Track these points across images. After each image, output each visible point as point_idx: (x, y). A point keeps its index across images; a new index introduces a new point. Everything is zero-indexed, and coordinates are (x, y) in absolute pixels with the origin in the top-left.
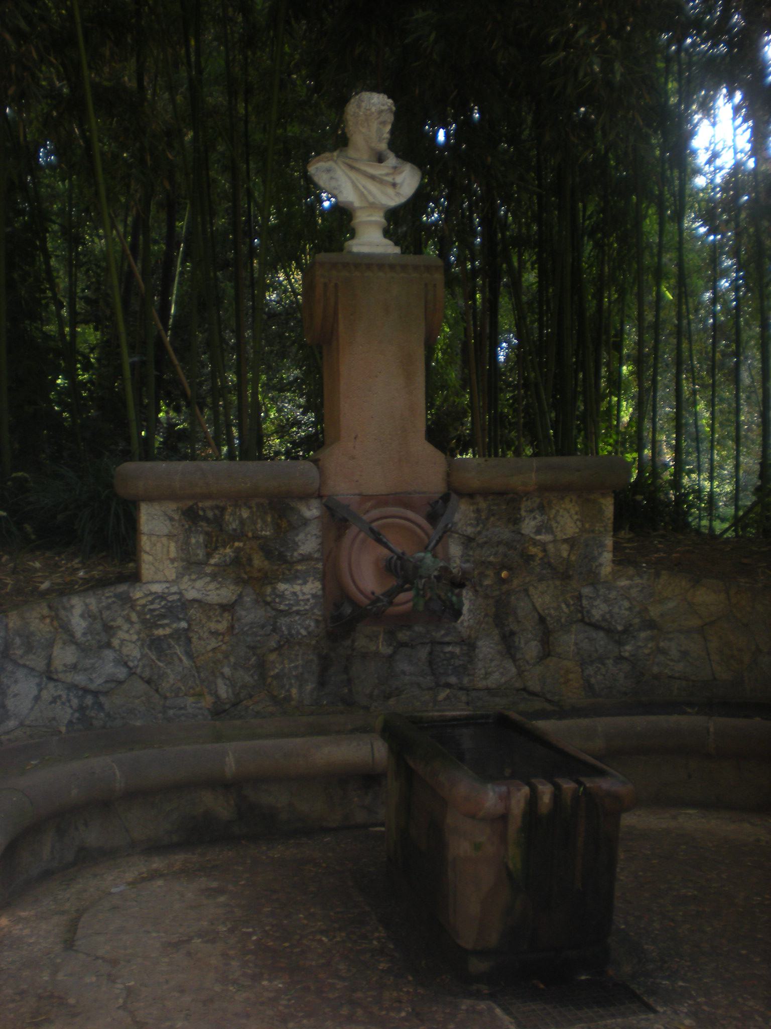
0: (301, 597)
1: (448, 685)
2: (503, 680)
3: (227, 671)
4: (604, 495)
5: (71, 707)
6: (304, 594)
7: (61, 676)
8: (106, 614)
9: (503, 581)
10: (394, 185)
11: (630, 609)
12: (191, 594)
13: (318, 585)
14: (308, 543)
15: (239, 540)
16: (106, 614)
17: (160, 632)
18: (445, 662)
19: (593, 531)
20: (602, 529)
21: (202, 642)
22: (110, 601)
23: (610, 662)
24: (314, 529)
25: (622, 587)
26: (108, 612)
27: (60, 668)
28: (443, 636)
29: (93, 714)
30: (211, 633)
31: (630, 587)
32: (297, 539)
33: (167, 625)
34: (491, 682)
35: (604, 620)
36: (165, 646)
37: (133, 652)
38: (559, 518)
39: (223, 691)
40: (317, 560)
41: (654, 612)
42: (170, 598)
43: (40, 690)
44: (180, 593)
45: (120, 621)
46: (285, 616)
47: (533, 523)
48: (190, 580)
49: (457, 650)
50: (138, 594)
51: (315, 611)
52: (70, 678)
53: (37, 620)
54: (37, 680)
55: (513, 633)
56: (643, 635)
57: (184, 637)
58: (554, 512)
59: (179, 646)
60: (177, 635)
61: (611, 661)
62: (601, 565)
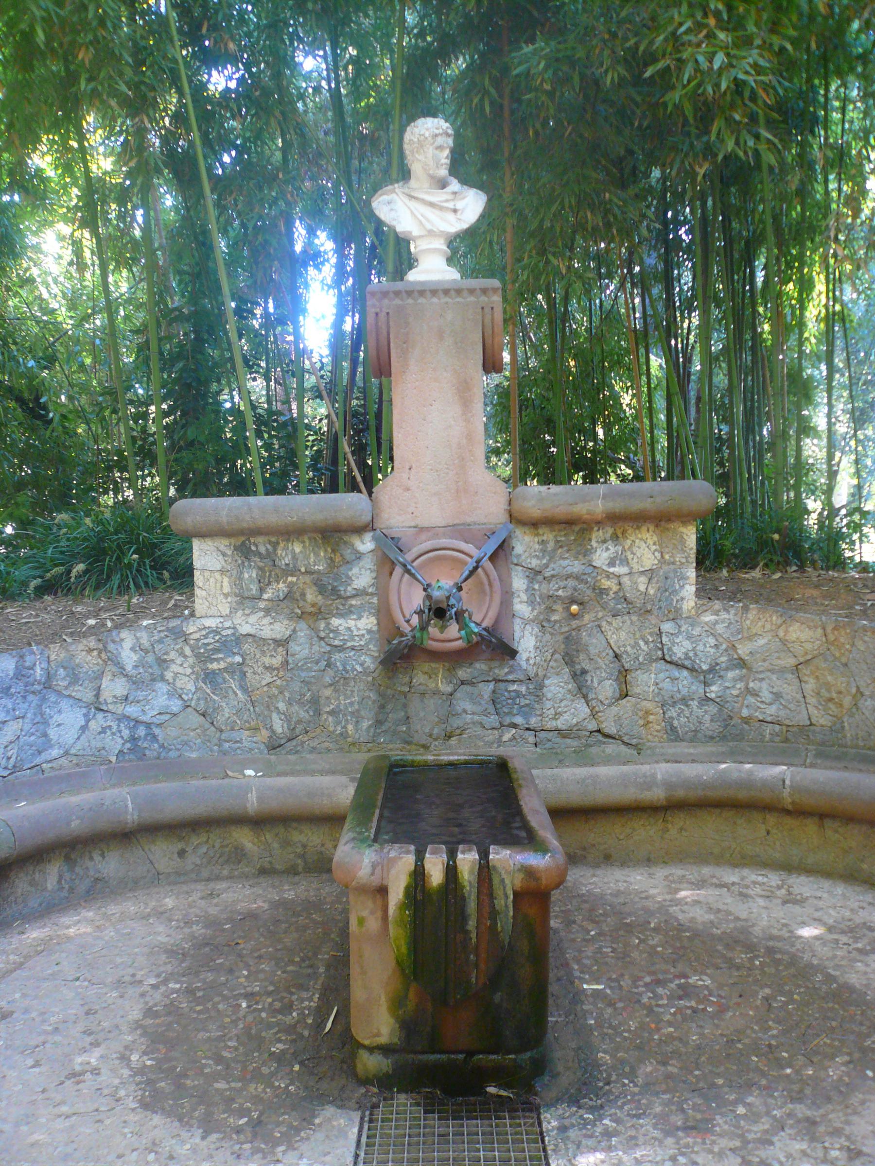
0: (355, 633)
1: (515, 726)
2: (574, 721)
3: (282, 706)
4: (685, 523)
5: (122, 737)
6: (359, 629)
7: (111, 707)
8: (158, 647)
9: (574, 616)
10: (455, 211)
11: (716, 646)
12: (245, 629)
13: (373, 620)
14: (362, 577)
15: (292, 575)
16: (158, 647)
17: (215, 666)
18: (510, 701)
19: (673, 563)
20: (684, 560)
21: (257, 677)
22: (162, 635)
23: (694, 704)
24: (368, 563)
25: (706, 623)
26: (160, 646)
27: (110, 700)
28: (506, 674)
29: (145, 745)
30: (266, 668)
31: (717, 622)
32: (350, 573)
33: (222, 659)
34: (560, 724)
35: (687, 656)
36: (220, 680)
37: (188, 685)
38: (635, 549)
39: (279, 726)
40: (372, 594)
41: (743, 650)
42: (224, 633)
43: (88, 721)
44: (234, 628)
45: (173, 655)
46: (340, 652)
47: (605, 555)
48: (244, 614)
49: (523, 689)
50: (191, 628)
51: (371, 646)
52: (119, 709)
53: (83, 654)
54: (84, 710)
55: (584, 672)
56: (730, 675)
57: (239, 671)
58: (629, 542)
59: (234, 680)
60: (230, 669)
61: (696, 703)
62: (682, 599)
